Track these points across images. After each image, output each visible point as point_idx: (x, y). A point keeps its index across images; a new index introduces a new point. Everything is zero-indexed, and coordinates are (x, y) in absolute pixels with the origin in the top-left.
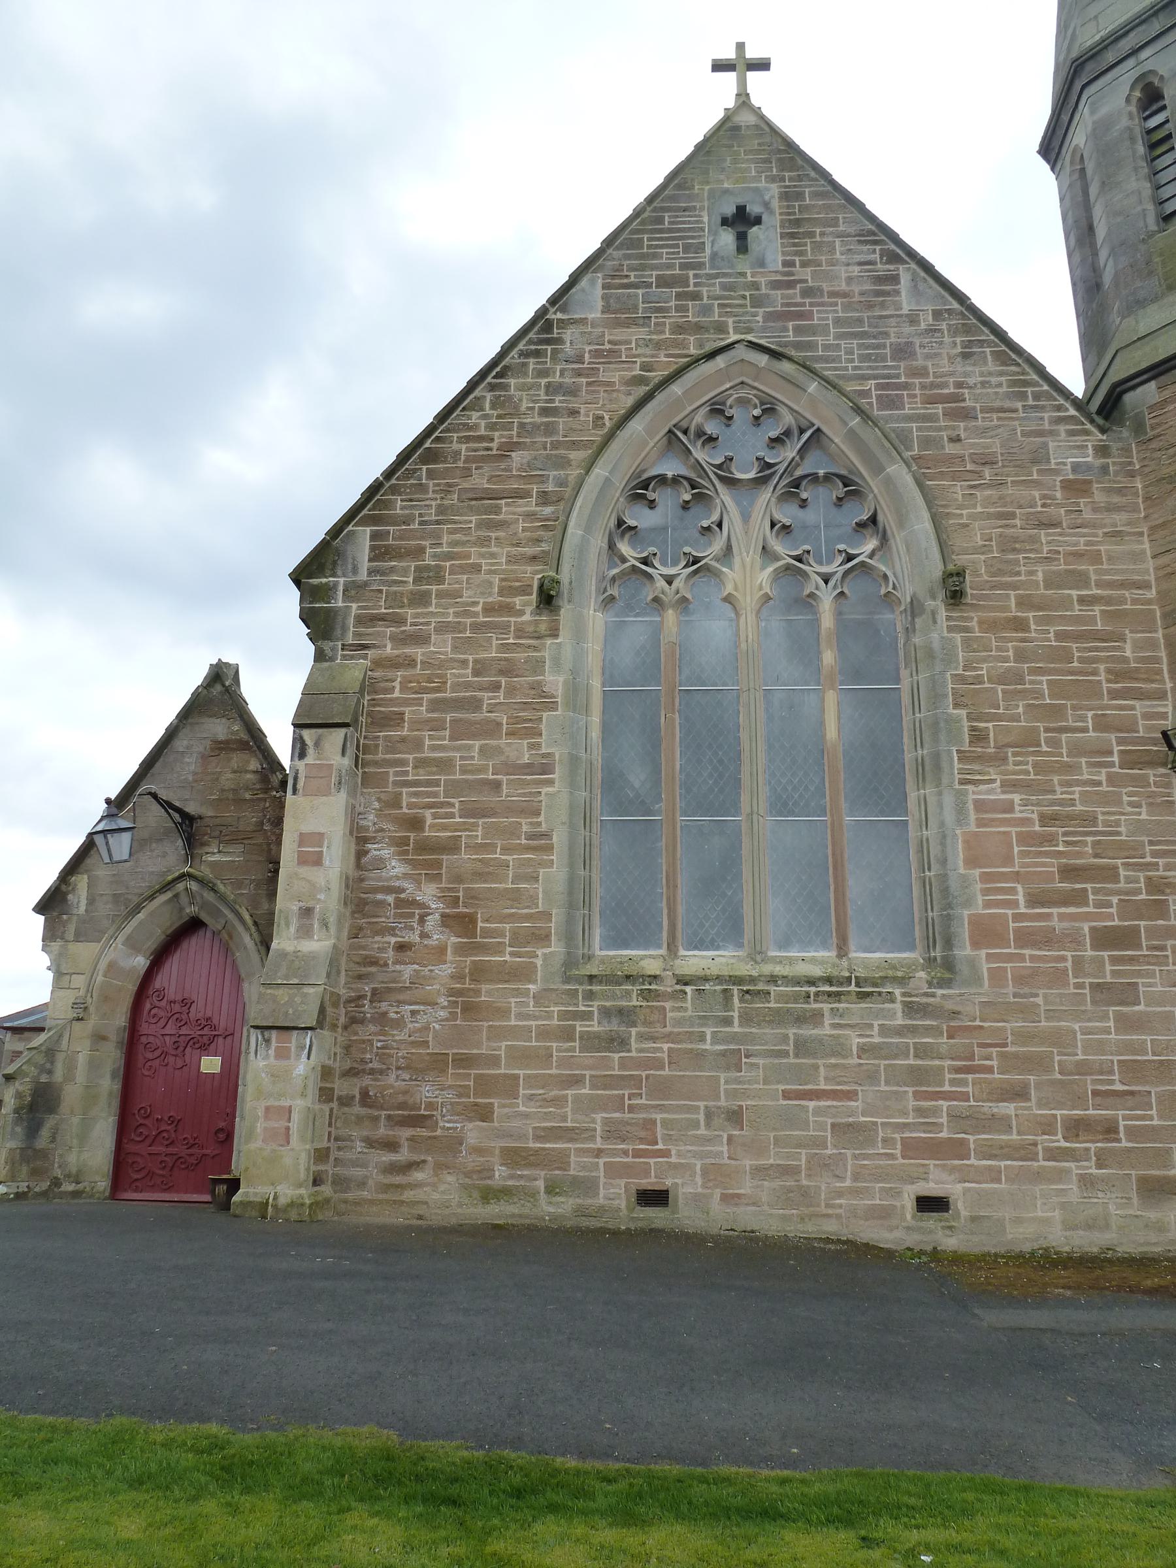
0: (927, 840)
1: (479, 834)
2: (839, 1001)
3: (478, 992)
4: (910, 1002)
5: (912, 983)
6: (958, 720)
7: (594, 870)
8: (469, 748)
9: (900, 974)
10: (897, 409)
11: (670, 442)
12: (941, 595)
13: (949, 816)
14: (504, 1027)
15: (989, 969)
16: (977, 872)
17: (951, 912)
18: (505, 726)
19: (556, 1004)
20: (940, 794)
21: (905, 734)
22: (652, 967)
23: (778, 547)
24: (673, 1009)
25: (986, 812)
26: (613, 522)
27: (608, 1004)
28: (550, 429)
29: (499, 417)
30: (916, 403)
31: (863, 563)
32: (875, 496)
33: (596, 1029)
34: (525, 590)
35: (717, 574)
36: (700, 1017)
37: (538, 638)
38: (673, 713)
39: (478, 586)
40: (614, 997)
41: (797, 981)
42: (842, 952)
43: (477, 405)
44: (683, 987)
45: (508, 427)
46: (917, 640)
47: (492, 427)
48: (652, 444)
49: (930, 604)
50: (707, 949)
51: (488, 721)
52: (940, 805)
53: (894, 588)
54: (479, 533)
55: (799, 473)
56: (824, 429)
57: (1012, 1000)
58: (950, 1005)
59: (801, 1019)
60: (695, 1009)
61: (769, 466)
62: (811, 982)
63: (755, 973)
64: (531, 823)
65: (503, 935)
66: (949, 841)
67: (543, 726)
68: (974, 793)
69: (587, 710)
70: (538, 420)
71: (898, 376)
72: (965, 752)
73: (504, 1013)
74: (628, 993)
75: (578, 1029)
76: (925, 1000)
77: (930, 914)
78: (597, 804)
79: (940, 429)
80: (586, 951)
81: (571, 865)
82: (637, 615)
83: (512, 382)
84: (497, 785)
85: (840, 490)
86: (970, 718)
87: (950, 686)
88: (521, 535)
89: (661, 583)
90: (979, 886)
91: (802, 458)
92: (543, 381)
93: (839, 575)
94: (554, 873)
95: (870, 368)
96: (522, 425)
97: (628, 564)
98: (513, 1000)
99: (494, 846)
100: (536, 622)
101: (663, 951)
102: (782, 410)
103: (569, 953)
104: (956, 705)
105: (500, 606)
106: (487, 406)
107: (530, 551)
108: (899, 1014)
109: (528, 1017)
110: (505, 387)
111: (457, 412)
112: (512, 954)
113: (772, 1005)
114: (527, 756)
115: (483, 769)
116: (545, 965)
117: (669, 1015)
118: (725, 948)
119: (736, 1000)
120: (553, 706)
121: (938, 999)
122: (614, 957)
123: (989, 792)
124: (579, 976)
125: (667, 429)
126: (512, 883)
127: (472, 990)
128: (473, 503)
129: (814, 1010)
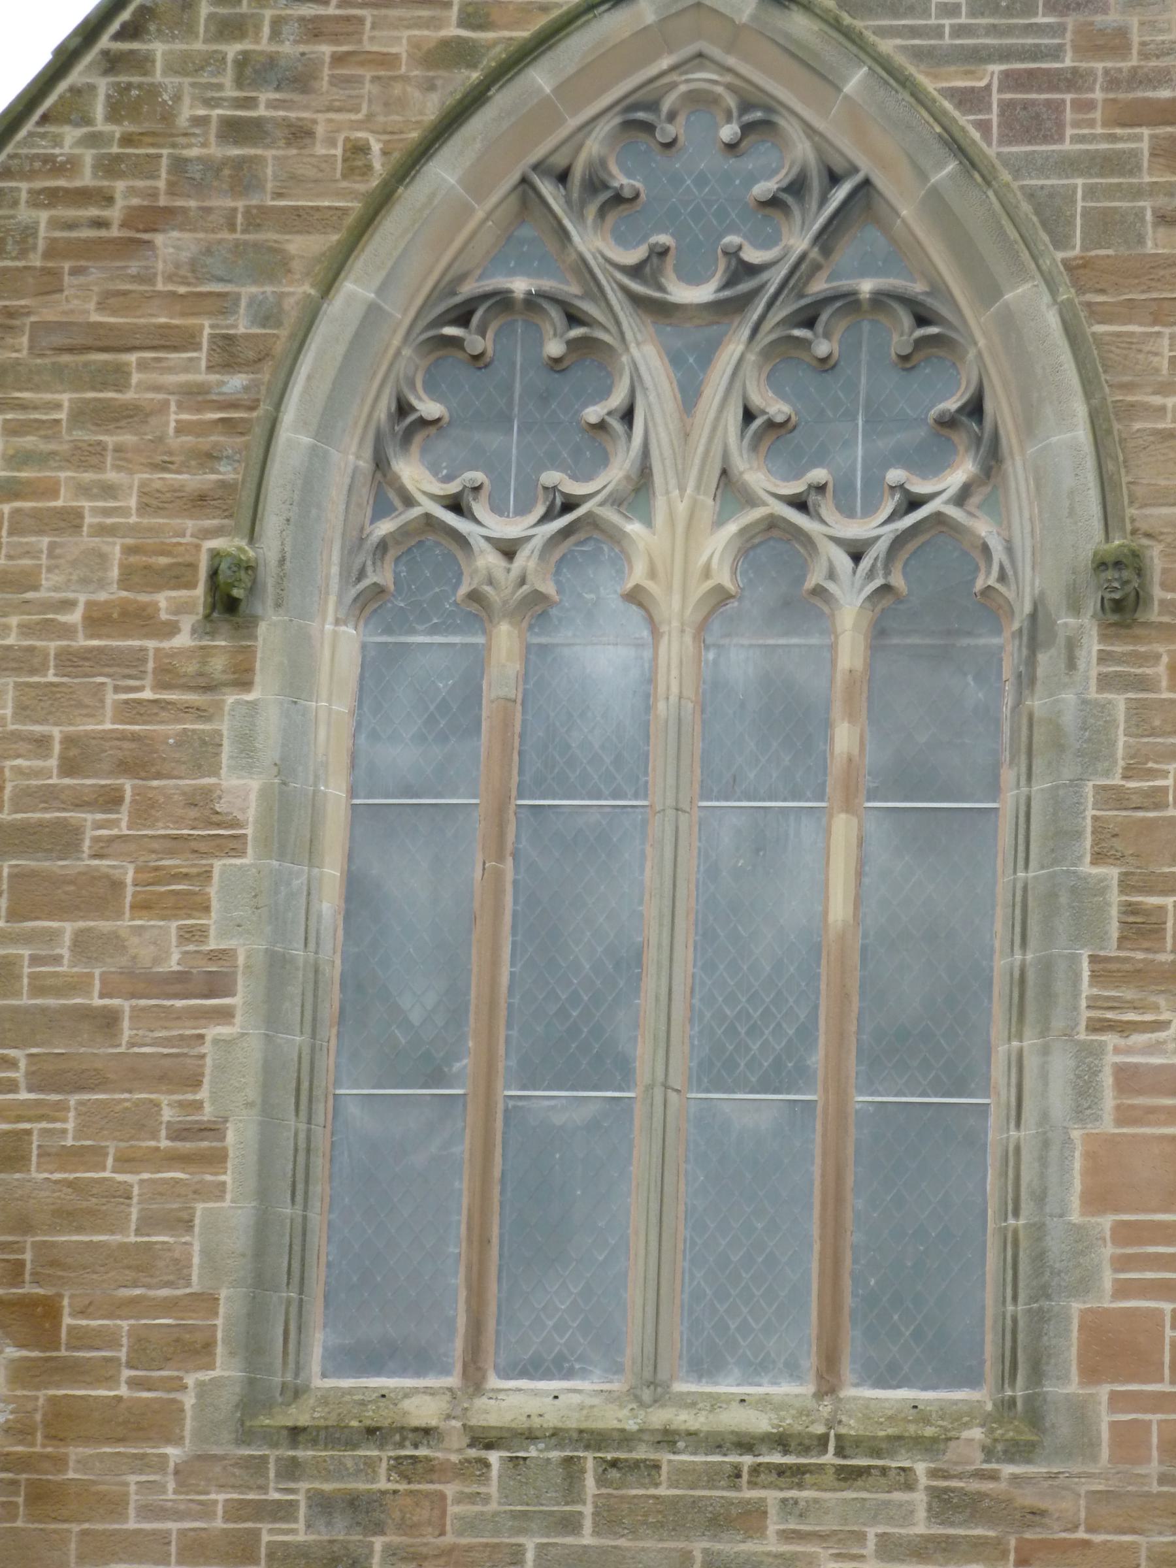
0: (1018, 1149)
1: (70, 1126)
2: (800, 1486)
3: (60, 1462)
4: (946, 1490)
5: (953, 1452)
6: (1100, 889)
7: (316, 1204)
8: (52, 937)
9: (929, 1431)
10: (1046, 139)
11: (524, 204)
12: (1092, 604)
13: (1059, 1099)
14: (114, 1533)
15: (1113, 1425)
16: (1107, 1221)
17: (1046, 1304)
18: (130, 890)
19: (222, 1487)
20: (1045, 1051)
21: (1000, 913)
22: (424, 1410)
23: (757, 477)
24: (461, 1498)
25: (1140, 1092)
26: (385, 407)
27: (327, 1487)
28: (243, 176)
29: (127, 140)
30: (1091, 123)
31: (938, 518)
32: (980, 355)
33: (301, 1537)
34: (179, 577)
35: (616, 537)
36: (514, 1515)
37: (208, 688)
38: (500, 858)
39: (74, 563)
40: (339, 1472)
41: (717, 1443)
42: (828, 1386)
43: (74, 110)
44: (483, 1454)
45: (146, 167)
46: (1037, 703)
47: (110, 167)
48: (480, 214)
49: (1066, 622)
50: (547, 1375)
51: (92, 878)
52: (1044, 1076)
53: (1002, 577)
54: (78, 434)
55: (819, 286)
56: (879, 181)
57: (1155, 1488)
58: (1027, 1498)
59: (720, 1521)
60: (506, 1497)
61: (752, 270)
62: (746, 1444)
63: (631, 1426)
64: (181, 1104)
65: (114, 1343)
66: (1054, 1153)
67: (213, 891)
68: (1117, 1050)
69: (312, 852)
70: (217, 151)
71: (1056, 53)
72: (1107, 959)
73: (115, 1505)
74: (370, 1464)
75: (266, 1538)
76: (975, 1486)
77: (1010, 1308)
78: (328, 1062)
79: (1138, 192)
80: (289, 1378)
81: (264, 1194)
82: (434, 630)
83: (159, 49)
84: (108, 1021)
85: (902, 333)
86: (1125, 885)
87: (1090, 812)
88: (175, 442)
89: (489, 559)
90: (1109, 1251)
91: (826, 251)
92: (232, 50)
93: (881, 547)
94: (228, 1211)
95: (993, 30)
96: (179, 165)
97: (415, 512)
98: (133, 1479)
99: (101, 1152)
100: (204, 653)
101: (453, 1380)
102: (789, 127)
103: (251, 1382)
104: (1099, 858)
105: (124, 613)
106: (99, 110)
107: (193, 480)
108: (921, 1513)
109: (160, 1512)
110: (142, 63)
111: (29, 126)
112: (134, 1383)
113: (662, 1491)
114: (175, 957)
115: (79, 985)
116: (200, 1407)
117: (453, 1509)
118: (584, 1374)
119: (590, 1481)
120: (234, 846)
121: (1002, 1486)
122: (351, 1391)
123: (1150, 1049)
124: (270, 1428)
125: (515, 177)
126: (138, 1232)
127: (47, 1457)
128: (66, 358)
129: (749, 1502)
